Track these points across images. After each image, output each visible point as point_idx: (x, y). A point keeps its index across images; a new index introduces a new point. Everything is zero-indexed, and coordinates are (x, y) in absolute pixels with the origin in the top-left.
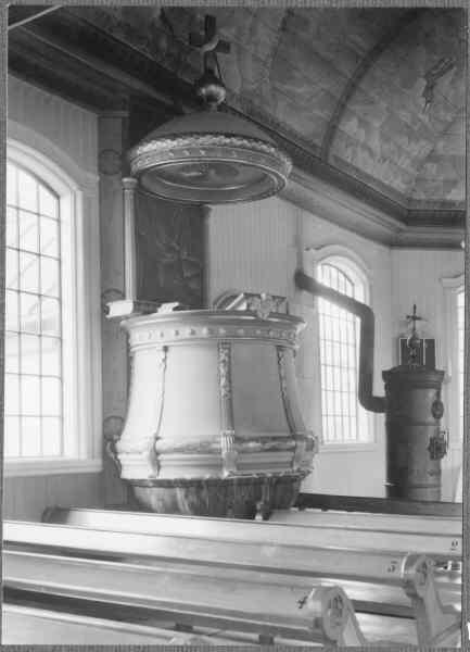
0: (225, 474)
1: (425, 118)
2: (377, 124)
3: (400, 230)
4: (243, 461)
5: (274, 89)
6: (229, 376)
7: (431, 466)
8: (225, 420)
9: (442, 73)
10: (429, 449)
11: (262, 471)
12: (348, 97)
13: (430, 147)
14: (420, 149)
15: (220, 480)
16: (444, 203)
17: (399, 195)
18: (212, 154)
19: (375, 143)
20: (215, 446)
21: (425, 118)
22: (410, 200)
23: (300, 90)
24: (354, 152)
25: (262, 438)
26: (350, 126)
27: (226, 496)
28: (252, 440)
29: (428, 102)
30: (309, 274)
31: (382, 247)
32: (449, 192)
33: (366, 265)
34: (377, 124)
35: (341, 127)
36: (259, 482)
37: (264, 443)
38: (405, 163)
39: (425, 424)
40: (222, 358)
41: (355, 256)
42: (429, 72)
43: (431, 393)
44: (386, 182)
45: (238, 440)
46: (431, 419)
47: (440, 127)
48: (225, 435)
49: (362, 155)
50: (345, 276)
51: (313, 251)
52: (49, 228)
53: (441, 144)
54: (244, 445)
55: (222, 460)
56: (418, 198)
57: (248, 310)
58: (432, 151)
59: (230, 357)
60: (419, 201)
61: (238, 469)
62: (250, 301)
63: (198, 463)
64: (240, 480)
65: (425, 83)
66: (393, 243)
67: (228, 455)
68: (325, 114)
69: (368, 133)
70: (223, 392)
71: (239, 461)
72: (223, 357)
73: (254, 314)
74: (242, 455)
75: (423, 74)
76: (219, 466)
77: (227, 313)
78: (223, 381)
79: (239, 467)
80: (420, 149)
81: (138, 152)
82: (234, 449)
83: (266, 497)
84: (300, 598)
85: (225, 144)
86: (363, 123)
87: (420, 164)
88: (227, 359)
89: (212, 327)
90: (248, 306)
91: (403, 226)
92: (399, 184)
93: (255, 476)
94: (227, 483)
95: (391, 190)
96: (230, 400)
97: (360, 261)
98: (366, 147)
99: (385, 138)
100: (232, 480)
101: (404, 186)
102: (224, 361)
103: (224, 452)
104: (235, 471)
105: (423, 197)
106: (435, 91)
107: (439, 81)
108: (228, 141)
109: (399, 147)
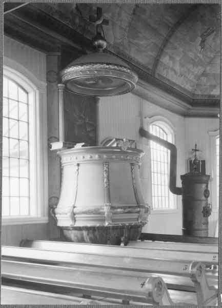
0: (106, 224)
1: (201, 56)
2: (178, 59)
3: (189, 109)
4: (115, 218)
5: (130, 42)
6: (108, 177)
7: (203, 220)
8: (106, 198)
9: (209, 35)
10: (203, 212)
11: (124, 223)
12: (164, 46)
13: (203, 69)
14: (198, 70)
15: (104, 227)
16: (210, 96)
17: (189, 92)
18: (100, 73)
19: (177, 67)
20: (101, 211)
21: (201, 56)
22: (194, 94)
23: (142, 43)
24: (167, 72)
25: (124, 207)
26: (165, 60)
27: (107, 234)
28: (119, 208)
29: (202, 48)
30: (146, 130)
31: (180, 117)
32: (212, 91)
33: (173, 125)
34: (178, 59)
35: (161, 60)
36: (122, 228)
37: (125, 209)
38: (191, 77)
39: (201, 200)
40: (105, 169)
41: (168, 121)
42: (203, 34)
43: (204, 186)
44: (183, 86)
45: (112, 208)
46: (203, 198)
47: (208, 60)
48: (106, 205)
49: (171, 73)
50: (163, 130)
51: (148, 119)
52: (23, 108)
53: (208, 68)
54: (115, 210)
55: (105, 217)
56: (197, 94)
57: (117, 146)
58: (204, 71)
59: (108, 169)
60: (198, 95)
61: (113, 222)
62: (118, 142)
63: (94, 219)
64: (113, 227)
65: (201, 39)
66: (185, 115)
67: (108, 215)
68: (153, 54)
69: (174, 63)
70: (105, 185)
71: (113, 218)
72: (105, 168)
73: (120, 148)
74: (114, 215)
75: (200, 35)
76: (103, 220)
77: (107, 148)
78: (105, 180)
79: (113, 220)
80: (198, 70)
81: (65, 72)
82: (111, 212)
83: (126, 235)
84: (142, 282)
85: (106, 68)
86: (171, 58)
87: (198, 78)
88: (107, 170)
89: (100, 154)
90: (117, 144)
91: (190, 107)
92: (188, 87)
93: (120, 225)
94: (107, 228)
95: (185, 90)
96: (109, 189)
97: (170, 123)
98: (173, 70)
99: (182, 65)
100: (110, 227)
101: (191, 88)
102: (106, 171)
103: (106, 214)
104: (111, 222)
105: (200, 93)
106: (205, 43)
107: (207, 38)
108: (108, 66)
109: (189, 70)
